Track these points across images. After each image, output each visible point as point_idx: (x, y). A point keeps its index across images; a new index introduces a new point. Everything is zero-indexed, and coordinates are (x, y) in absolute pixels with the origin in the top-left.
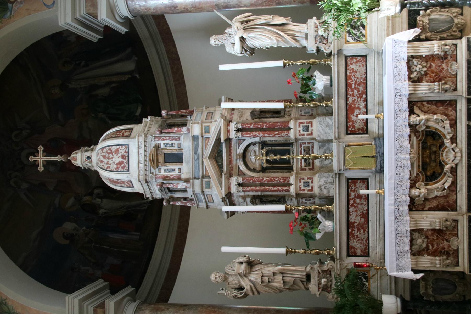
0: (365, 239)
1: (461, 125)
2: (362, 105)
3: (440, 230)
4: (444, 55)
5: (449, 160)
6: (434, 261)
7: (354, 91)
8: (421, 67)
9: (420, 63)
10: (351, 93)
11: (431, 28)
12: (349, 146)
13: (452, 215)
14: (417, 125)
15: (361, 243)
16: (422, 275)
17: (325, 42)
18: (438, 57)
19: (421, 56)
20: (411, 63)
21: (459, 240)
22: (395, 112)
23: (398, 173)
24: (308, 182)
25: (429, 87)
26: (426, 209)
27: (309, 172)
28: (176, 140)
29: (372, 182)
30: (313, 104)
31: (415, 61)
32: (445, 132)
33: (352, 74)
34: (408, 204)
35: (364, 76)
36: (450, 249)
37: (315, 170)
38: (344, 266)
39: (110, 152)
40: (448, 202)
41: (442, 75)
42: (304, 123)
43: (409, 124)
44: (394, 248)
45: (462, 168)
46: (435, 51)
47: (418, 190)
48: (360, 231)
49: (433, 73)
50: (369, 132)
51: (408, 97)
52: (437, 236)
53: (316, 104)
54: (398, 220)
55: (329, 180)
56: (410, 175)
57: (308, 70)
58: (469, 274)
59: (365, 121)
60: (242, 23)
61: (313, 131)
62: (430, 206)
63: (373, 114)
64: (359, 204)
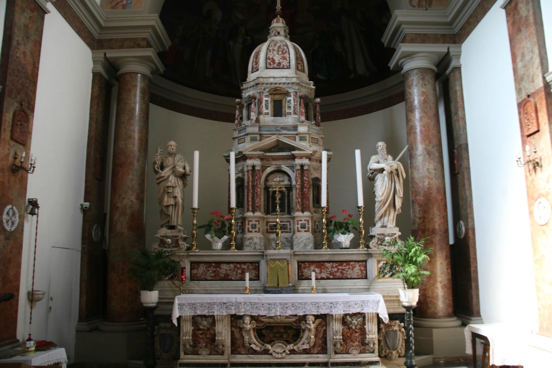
2: (324, 275)
3: (215, 340)
4: (365, 343)
10: (334, 265)
12: (288, 264)
13: (228, 350)
14: (306, 321)
16: (176, 324)
17: (379, 242)
19: (365, 324)
20: (359, 316)
22: (317, 303)
26: (233, 329)
27: (265, 229)
28: (294, 111)
29: (256, 284)
32: (299, 345)
34: (237, 314)
35: (349, 277)
39: (284, 52)
40: (239, 347)
41: (348, 341)
42: (308, 224)
43: (306, 315)
44: (199, 302)
49: (351, 334)
51: (330, 313)
53: (325, 235)
56: (263, 316)
57: (354, 228)
59: (309, 277)
60: (397, 170)
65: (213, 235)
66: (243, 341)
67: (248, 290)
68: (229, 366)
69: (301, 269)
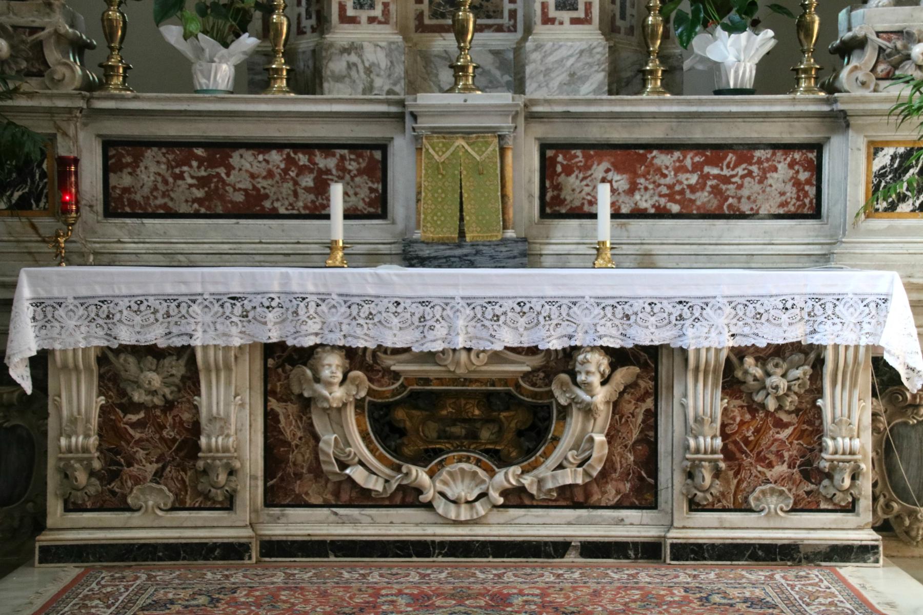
0: (170, 204)
1: (569, 524)
2: (645, 202)
3: (198, 448)
4: (819, 471)
5: (445, 483)
6: (80, 429)
7: (693, 171)
8: (781, 392)
9: (796, 388)
10: (688, 162)
11: (902, 430)
12: (502, 151)
14: (573, 375)
15: (156, 188)
16: (27, 386)
17: (881, 68)
18: (812, 450)
19: (819, 392)
20: (797, 357)
21: (160, 513)
22: (623, 301)
23: (400, 309)
24: (372, 7)
25: (707, 419)
26: (273, 403)
27: (412, 15)
29: (371, 231)
30: (654, 26)
31: (802, 372)
32: (544, 471)
33: (754, 168)
34: (290, 342)
35: (745, 208)
36: (129, 484)
37: (416, 37)
38: (63, 125)
40: (299, 476)
43: (576, 349)
44: (125, 291)
45: (417, 525)
46: (834, 439)
47: (340, 376)
48: (198, 187)
49: (757, 431)
50: (548, 221)
51: (676, 344)
52: (174, 440)
53: (654, 36)
54: (228, 305)
55: (378, 82)
56: (396, 351)
57: (777, 8)
58: (37, 545)
59: (586, 208)
61: (556, 26)
62: (282, 418)
63: (612, 237)
64: (296, 183)
65: (194, 27)
66: (316, 451)
67: (340, 254)
68: (254, 554)
69: (555, 174)
